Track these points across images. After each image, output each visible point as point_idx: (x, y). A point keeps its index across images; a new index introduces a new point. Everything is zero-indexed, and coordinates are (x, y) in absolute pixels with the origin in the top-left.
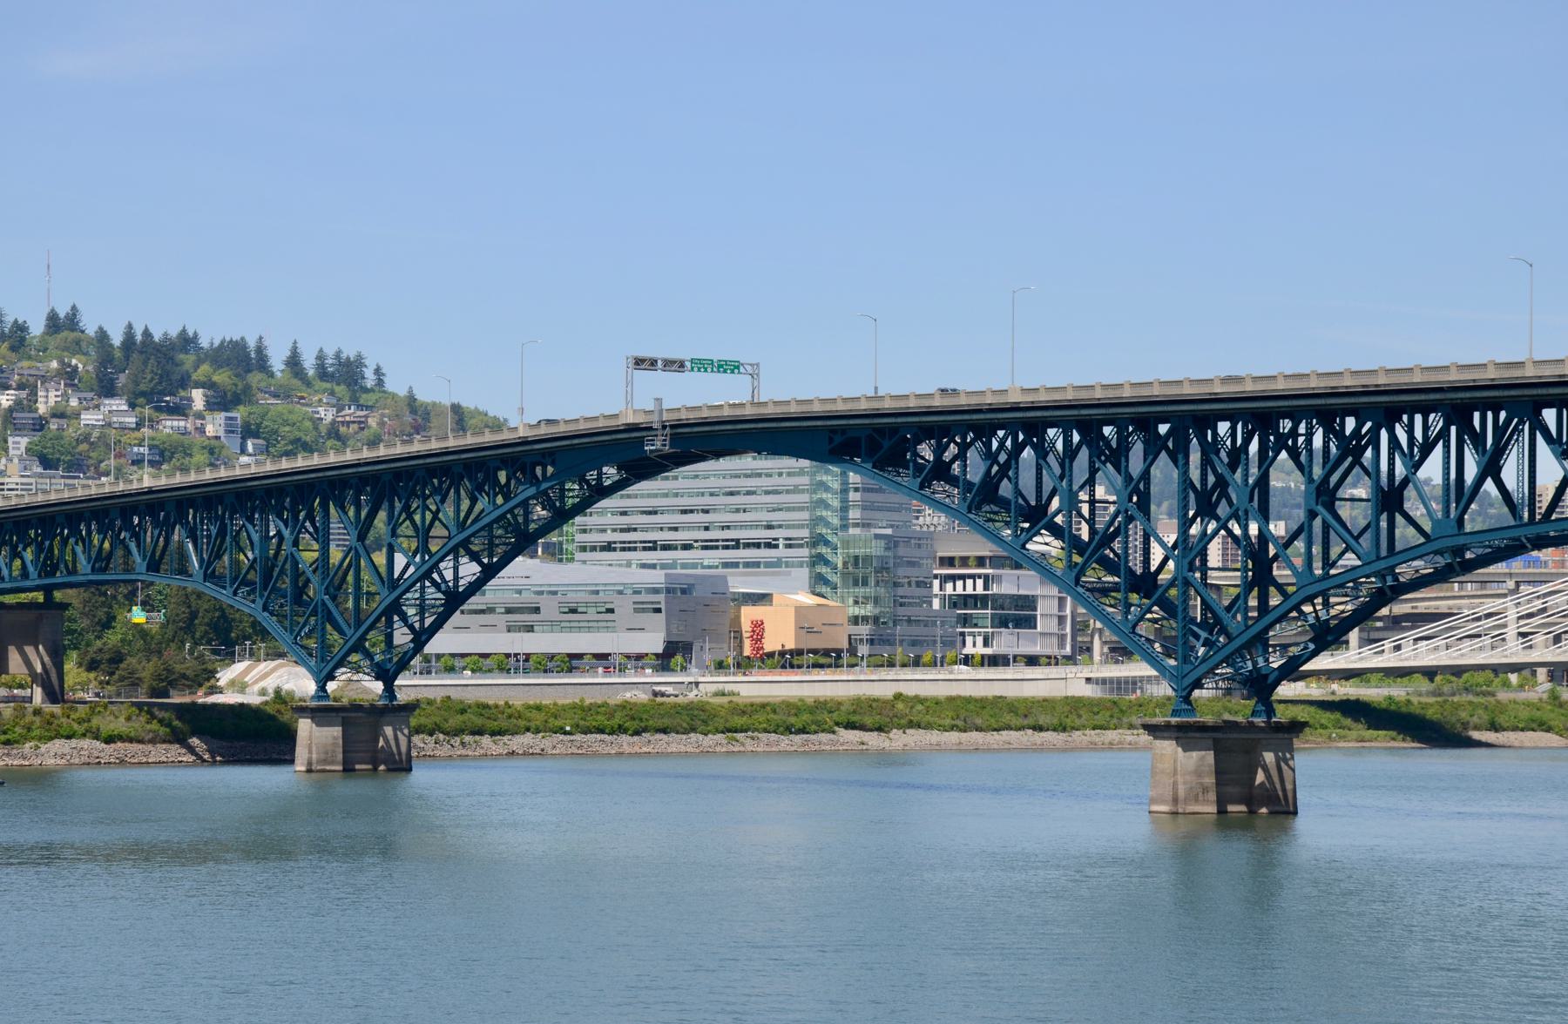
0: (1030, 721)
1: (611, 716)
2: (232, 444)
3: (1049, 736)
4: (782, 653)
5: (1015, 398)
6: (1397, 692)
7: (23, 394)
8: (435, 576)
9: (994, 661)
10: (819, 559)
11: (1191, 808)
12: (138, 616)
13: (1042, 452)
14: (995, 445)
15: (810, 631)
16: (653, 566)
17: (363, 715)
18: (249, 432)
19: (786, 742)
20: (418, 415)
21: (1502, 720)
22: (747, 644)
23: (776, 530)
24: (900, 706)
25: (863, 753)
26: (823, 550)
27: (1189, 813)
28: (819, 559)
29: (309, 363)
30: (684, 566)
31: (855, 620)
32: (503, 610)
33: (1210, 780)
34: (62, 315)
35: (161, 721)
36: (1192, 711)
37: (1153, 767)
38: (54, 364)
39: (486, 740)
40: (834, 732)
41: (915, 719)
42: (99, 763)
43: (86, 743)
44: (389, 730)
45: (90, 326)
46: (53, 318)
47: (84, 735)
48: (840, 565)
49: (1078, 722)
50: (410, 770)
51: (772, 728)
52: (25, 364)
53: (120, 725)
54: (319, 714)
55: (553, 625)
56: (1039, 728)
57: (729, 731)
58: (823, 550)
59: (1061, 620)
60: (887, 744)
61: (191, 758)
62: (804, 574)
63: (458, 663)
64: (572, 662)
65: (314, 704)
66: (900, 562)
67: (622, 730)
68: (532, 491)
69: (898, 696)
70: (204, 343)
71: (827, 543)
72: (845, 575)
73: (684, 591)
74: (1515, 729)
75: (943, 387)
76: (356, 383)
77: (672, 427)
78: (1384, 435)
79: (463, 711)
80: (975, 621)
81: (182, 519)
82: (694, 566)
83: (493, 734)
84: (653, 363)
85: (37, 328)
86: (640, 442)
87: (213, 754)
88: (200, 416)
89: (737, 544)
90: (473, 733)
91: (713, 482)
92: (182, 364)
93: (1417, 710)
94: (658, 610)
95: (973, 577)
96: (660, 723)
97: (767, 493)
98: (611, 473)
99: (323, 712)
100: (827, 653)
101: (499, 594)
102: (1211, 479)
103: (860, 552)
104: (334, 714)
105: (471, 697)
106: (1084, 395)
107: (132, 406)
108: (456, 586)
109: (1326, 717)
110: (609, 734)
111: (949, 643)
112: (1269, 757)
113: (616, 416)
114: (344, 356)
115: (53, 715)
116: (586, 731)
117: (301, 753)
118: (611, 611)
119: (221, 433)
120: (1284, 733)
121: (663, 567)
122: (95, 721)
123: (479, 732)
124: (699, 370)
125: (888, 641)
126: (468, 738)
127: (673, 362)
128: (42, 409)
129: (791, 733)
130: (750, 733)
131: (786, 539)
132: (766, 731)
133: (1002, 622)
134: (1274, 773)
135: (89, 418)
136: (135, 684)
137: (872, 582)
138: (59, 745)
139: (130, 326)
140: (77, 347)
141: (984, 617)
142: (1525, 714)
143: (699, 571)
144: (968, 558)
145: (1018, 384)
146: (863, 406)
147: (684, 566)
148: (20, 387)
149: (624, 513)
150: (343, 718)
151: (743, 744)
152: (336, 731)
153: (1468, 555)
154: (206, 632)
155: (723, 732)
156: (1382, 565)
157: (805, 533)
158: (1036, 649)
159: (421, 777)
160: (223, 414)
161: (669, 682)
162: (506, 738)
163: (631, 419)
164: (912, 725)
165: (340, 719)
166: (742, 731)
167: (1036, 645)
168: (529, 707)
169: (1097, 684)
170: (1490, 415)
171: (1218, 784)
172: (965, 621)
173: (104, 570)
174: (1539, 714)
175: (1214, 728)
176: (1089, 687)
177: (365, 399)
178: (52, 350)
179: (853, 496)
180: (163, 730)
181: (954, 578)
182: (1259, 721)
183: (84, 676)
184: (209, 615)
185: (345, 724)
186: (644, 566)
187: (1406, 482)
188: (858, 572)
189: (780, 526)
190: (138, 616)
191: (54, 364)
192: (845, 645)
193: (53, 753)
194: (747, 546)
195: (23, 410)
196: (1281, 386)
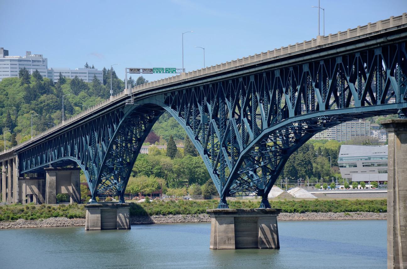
17: (109, 208)
27: (220, 249)
32: (377, 165)
33: (232, 235)
42: (309, 220)
51: (371, 210)
54: (90, 208)
57: (347, 211)
77: (136, 95)
96: (314, 209)
101: (375, 159)
104: (97, 208)
110: (289, 213)
120: (270, 214)
124: (157, 72)
129: (380, 212)
130: (358, 212)
150: (101, 210)
151: (352, 217)
154: (287, 175)
155: (344, 212)
184: (288, 168)
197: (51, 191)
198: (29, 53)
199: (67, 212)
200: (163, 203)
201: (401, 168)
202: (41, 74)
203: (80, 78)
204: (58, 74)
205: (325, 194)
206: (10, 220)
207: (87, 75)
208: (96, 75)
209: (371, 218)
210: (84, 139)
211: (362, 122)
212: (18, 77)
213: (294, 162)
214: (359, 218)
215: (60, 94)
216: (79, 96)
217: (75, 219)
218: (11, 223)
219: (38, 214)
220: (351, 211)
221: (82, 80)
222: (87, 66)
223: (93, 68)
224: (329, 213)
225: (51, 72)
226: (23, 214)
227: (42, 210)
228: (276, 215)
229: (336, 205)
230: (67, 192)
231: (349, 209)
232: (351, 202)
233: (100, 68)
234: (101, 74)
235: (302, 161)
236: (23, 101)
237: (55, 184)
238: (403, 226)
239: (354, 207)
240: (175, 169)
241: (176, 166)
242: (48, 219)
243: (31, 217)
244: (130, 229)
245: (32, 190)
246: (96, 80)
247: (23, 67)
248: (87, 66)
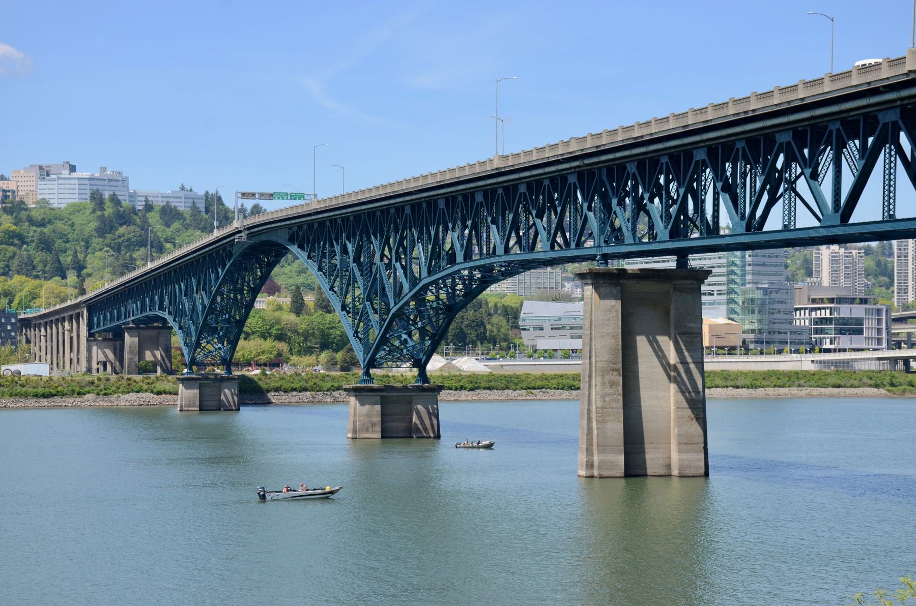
15: (718, 337)
19: (45, 402)
23: (713, 286)
32: (568, 328)
33: (377, 419)
48: (741, 303)
57: (529, 388)
59: (879, 331)
62: (724, 308)
66: (772, 301)
71: (736, 293)
72: (743, 309)
80: (826, 331)
95: (824, 308)
96: (487, 385)
120: (430, 392)
124: (279, 198)
129: (572, 389)
130: (544, 390)
131: (718, 291)
133: (841, 332)
137: (756, 312)
144: (823, 299)
150: (200, 384)
151: (536, 396)
155: (525, 389)
165: (198, 384)
167: (863, 344)
169: (817, 363)
172: (822, 331)
175: (378, 390)
176: (813, 365)
179: (748, 268)
181: (816, 309)
184: (454, 331)
188: (750, 306)
189: (715, 284)
197: (132, 356)
198: (103, 169)
199: (153, 386)
200: (285, 376)
201: (599, 333)
202: (120, 198)
203: (173, 204)
204: (144, 199)
205: (502, 366)
206: (75, 395)
207: (183, 200)
208: (195, 201)
209: (560, 397)
210: (177, 287)
211: (551, 271)
212: (88, 201)
213: (462, 323)
214: (544, 398)
215: (144, 226)
216: (171, 229)
217: (163, 395)
218: (77, 400)
219: (113, 388)
220: (534, 388)
221: (175, 207)
222: (183, 188)
223: (191, 190)
224: (506, 391)
225: (133, 196)
226: (93, 387)
227: (120, 383)
228: (436, 393)
229: (516, 381)
231: (532, 385)
232: (535, 376)
234: (202, 199)
235: (473, 321)
236: (95, 234)
237: (137, 348)
238: (599, 408)
239: (539, 383)
240: (301, 331)
241: (303, 326)
242: (127, 395)
243: (104, 392)
244: (239, 410)
245: (106, 356)
246: (194, 207)
247: (95, 188)
248: (183, 188)
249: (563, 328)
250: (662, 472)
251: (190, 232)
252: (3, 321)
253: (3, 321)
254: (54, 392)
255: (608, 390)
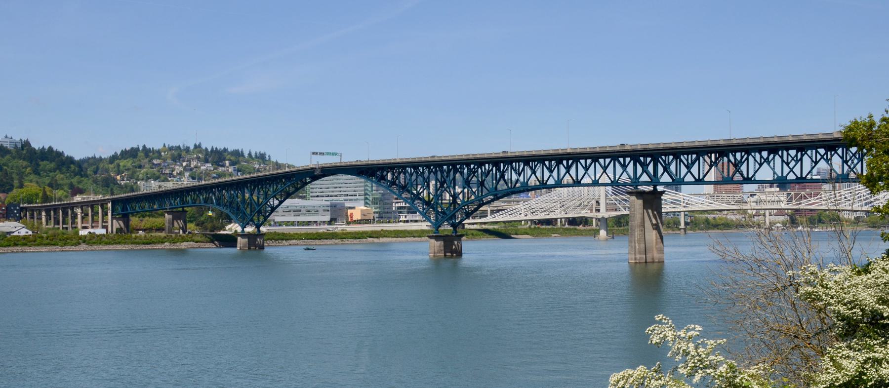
0: (412, 235)
1: (314, 236)
2: (235, 173)
3: (416, 239)
4: (358, 220)
5: (398, 161)
6: (496, 227)
7: (188, 163)
8: (268, 203)
9: (407, 221)
10: (366, 199)
11: (438, 255)
12: (210, 213)
13: (442, 171)
14: (395, 171)
16: (328, 201)
18: (239, 170)
19: (355, 241)
20: (278, 165)
21: (518, 233)
22: (349, 218)
24: (382, 232)
25: (373, 243)
26: (367, 196)
28: (366, 199)
29: (253, 155)
30: (335, 200)
31: (375, 212)
33: (442, 248)
34: (197, 145)
35: (208, 238)
36: (438, 232)
37: (430, 245)
38: (195, 156)
39: (284, 242)
40: (366, 239)
41: (386, 235)
43: (191, 243)
44: (258, 239)
45: (203, 147)
46: (195, 145)
47: (191, 241)
49: (423, 235)
50: (264, 248)
52: (189, 156)
53: (199, 239)
55: (305, 215)
56: (414, 237)
58: (367, 196)
60: (379, 241)
61: (215, 246)
62: (363, 202)
63: (282, 224)
64: (308, 223)
65: (241, 233)
67: (316, 239)
68: (290, 184)
69: (382, 230)
70: (229, 150)
71: (368, 195)
72: (372, 202)
73: (334, 206)
74: (521, 234)
75: (504, 151)
76: (264, 159)
78: (701, 158)
79: (279, 235)
81: (189, 195)
82: (337, 200)
83: (286, 240)
84: (317, 153)
85: (192, 148)
86: (314, 172)
87: (220, 245)
88: (228, 167)
89: (347, 195)
90: (281, 240)
91: (342, 181)
92: (224, 155)
93: (500, 231)
94: (329, 211)
96: (325, 237)
97: (354, 183)
98: (308, 180)
99: (243, 235)
100: (368, 220)
102: (443, 180)
103: (376, 197)
105: (280, 231)
106: (413, 160)
107: (212, 165)
108: (273, 206)
109: (480, 233)
111: (395, 218)
112: (456, 242)
113: (308, 166)
114: (261, 153)
115: (184, 236)
116: (308, 239)
117: (238, 245)
118: (318, 211)
119: (233, 171)
121: (330, 201)
122: (193, 238)
123: (283, 240)
125: (382, 217)
126: (280, 241)
127: (321, 153)
128: (192, 166)
132: (350, 239)
134: (457, 246)
135: (203, 168)
136: (207, 229)
138: (185, 243)
139: (212, 147)
140: (200, 152)
141: (405, 211)
142: (523, 231)
143: (339, 202)
145: (399, 158)
146: (338, 164)
147: (335, 200)
148: (188, 161)
149: (321, 188)
152: (247, 240)
153: (498, 196)
156: (479, 198)
157: (363, 192)
158: (417, 218)
159: (267, 250)
160: (233, 167)
161: (330, 228)
162: (289, 241)
163: (312, 167)
164: (386, 237)
166: (344, 239)
168: (294, 234)
170: (517, 163)
171: (445, 249)
172: (400, 212)
173: (195, 203)
174: (526, 231)
177: (266, 163)
178: (195, 153)
180: (209, 240)
181: (398, 202)
182: (454, 234)
183: (195, 227)
185: (249, 238)
186: (326, 201)
187: (484, 180)
188: (375, 202)
190: (210, 213)
191: (195, 156)
192: (372, 218)
193: (184, 245)
194: (350, 196)
195: (188, 166)
196: (457, 158)
203: (5, 146)
207: (9, 143)
208: (17, 144)
222: (6, 137)
223: (11, 138)
230: (119, 227)
233: (17, 138)
245: (120, 225)
246: (16, 147)
248: (6, 137)
249: (290, 211)
250: (652, 261)
251: (16, 160)
252: (12, 208)
253: (12, 208)
254: (151, 242)
255: (641, 233)
